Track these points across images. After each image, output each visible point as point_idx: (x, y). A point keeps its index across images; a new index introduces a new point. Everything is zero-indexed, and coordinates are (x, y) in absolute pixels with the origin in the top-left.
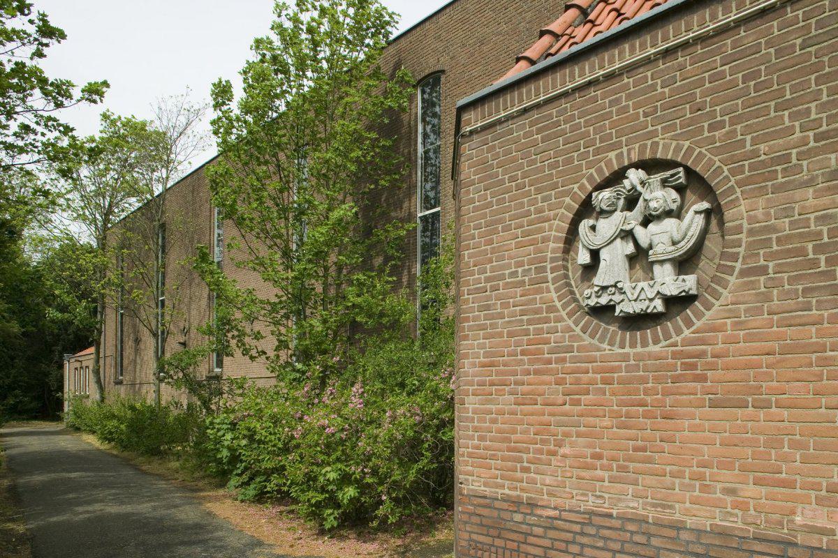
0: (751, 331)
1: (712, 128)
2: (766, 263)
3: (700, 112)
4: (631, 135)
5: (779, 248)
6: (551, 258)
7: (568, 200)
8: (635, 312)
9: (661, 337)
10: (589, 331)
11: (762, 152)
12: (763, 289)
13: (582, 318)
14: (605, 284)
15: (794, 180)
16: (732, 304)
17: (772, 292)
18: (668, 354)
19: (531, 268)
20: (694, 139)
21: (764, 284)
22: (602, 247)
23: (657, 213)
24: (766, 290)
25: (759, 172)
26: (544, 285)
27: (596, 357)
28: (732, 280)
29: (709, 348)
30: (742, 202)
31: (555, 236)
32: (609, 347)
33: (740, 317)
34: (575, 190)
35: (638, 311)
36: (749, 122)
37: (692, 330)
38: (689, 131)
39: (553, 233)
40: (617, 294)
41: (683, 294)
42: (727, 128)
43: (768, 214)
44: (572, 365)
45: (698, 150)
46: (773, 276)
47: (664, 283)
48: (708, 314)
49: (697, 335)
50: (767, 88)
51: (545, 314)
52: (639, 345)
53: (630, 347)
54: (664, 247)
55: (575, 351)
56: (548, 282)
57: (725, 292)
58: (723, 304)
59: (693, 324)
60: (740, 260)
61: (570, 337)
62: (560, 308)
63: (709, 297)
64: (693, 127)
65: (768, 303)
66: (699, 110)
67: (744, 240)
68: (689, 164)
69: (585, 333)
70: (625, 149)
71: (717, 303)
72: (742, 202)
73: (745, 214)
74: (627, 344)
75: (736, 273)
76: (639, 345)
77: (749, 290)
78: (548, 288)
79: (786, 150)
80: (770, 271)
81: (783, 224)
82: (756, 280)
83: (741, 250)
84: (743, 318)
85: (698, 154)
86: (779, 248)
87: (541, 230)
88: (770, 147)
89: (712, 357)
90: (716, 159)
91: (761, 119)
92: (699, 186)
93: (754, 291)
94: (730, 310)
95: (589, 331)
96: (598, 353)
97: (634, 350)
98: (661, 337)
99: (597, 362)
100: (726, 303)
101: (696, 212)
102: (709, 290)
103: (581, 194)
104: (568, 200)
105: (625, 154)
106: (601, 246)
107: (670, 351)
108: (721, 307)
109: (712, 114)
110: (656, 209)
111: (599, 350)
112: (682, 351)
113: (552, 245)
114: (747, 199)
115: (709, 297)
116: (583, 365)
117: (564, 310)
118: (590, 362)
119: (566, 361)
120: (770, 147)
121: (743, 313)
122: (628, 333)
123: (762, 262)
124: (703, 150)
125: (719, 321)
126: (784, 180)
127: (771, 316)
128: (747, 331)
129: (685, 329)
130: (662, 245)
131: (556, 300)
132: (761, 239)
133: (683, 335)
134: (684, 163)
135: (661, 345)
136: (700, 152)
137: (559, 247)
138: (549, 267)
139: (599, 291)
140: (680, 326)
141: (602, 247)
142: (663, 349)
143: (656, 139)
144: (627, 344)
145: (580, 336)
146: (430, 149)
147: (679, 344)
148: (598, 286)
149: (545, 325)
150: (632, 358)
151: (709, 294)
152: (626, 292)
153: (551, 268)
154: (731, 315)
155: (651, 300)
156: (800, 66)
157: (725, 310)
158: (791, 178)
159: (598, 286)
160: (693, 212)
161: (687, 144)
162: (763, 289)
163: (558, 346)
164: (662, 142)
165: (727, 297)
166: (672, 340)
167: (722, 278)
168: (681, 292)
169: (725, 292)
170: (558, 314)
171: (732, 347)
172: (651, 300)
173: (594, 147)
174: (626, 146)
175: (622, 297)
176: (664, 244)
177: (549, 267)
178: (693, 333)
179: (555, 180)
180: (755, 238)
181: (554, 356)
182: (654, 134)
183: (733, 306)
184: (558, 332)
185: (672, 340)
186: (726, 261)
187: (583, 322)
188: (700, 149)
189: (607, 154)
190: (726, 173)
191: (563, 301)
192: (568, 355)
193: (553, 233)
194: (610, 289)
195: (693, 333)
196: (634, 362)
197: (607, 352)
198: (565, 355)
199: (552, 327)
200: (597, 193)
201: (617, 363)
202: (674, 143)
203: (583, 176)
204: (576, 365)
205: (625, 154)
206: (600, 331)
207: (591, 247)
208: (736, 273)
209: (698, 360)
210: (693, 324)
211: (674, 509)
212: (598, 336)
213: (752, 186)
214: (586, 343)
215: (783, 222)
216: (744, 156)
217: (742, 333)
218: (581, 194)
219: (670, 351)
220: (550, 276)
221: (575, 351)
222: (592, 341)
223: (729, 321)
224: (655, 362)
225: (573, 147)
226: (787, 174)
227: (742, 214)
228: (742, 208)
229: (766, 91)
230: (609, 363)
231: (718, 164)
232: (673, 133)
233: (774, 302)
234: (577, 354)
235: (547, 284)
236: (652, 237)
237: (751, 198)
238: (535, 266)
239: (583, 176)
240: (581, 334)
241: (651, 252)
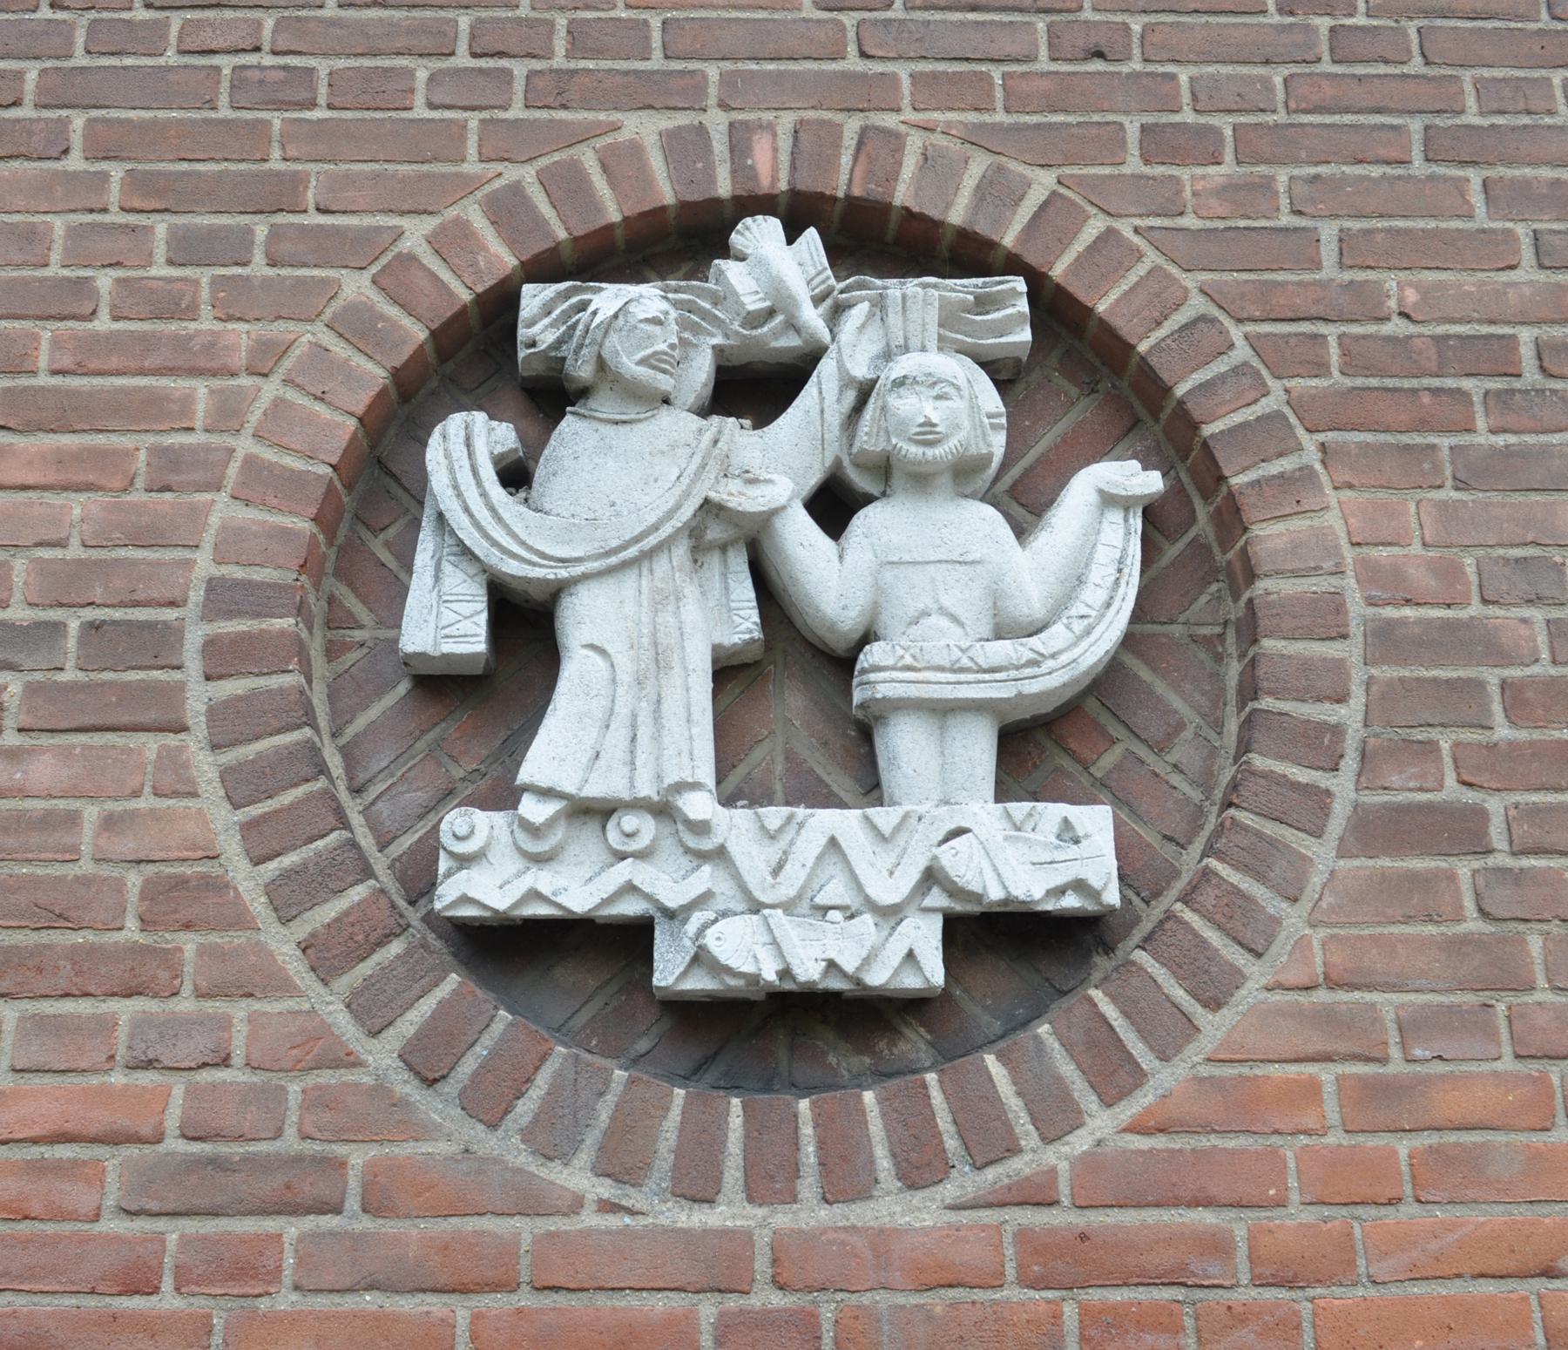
0: (1451, 1138)
1: (1157, 144)
2: (1470, 796)
3: (1098, 66)
4: (753, 66)
5: (1522, 735)
6: (213, 585)
7: (356, 286)
8: (785, 973)
9: (951, 1143)
10: (468, 1066)
11: (1392, 304)
12: (1473, 925)
13: (416, 979)
14: (596, 789)
15: (1545, 450)
16: (1332, 984)
17: (1521, 941)
18: (998, 1247)
19: (58, 628)
20: (1076, 170)
21: (1478, 896)
22: (586, 577)
23: (931, 452)
24: (1488, 928)
25: (1390, 383)
26: (151, 745)
27: (508, 1249)
28: (1321, 854)
29: (1239, 1226)
30: (1332, 496)
31: (250, 462)
32: (605, 1189)
33: (1383, 1060)
34: (406, 245)
35: (809, 971)
36: (1323, 170)
37: (1129, 1110)
38: (1051, 126)
39: (245, 445)
40: (669, 852)
41: (1071, 902)
42: (1227, 168)
43: (1452, 572)
44: (322, 1302)
45: (1095, 226)
46: (1509, 862)
47: (959, 832)
48: (1214, 1027)
49: (1160, 1142)
50: (1386, 62)
51: (132, 931)
52: (808, 1186)
53: (753, 1196)
54: (954, 635)
55: (353, 1203)
56: (184, 729)
57: (1293, 918)
58: (1291, 978)
59: (1139, 1077)
60: (1350, 764)
61: (316, 1100)
62: (258, 905)
63: (1213, 936)
64: (1071, 119)
65: (1511, 998)
66: (1100, 55)
67: (1358, 675)
68: (1058, 271)
69: (431, 1083)
70: (717, 122)
71: (1257, 974)
72: (1332, 496)
73: (1349, 554)
74: (733, 1174)
75: (1336, 825)
76: (808, 1186)
77: (1408, 919)
78: (173, 761)
79: (1492, 322)
80: (1497, 834)
81: (1524, 631)
82: (1436, 875)
83: (1350, 715)
84: (1396, 1066)
85: (1093, 248)
86: (1522, 735)
87: (174, 413)
88: (1425, 291)
89: (1259, 1282)
90: (1190, 281)
91: (1376, 171)
92: (1074, 391)
93: (1431, 929)
94: (1328, 1018)
95: (468, 1066)
96: (525, 1229)
97: (782, 1218)
98: (951, 1143)
99: (510, 1286)
100: (1304, 980)
101: (1109, 500)
102: (1208, 897)
103: (445, 275)
104: (356, 286)
105: (720, 146)
106: (578, 570)
107: (1009, 1230)
108: (1277, 997)
109: (1158, 92)
110: (928, 434)
111: (532, 1201)
112: (1083, 1237)
113: (222, 510)
114: (1350, 486)
115: (1213, 936)
116: (407, 1305)
117: (285, 921)
118: (463, 1290)
119: (275, 1274)
120: (1425, 291)
121: (1394, 1037)
122: (736, 1102)
123: (1452, 790)
124: (1125, 228)
125: (1275, 1070)
126: (1500, 440)
127: (1534, 1067)
128: (1432, 1139)
129: (1088, 1100)
130: (944, 622)
131: (232, 848)
132: (1435, 680)
133: (1079, 1142)
134: (1032, 258)
135: (949, 1190)
136: (1110, 232)
137: (285, 534)
138: (195, 636)
139: (551, 823)
140: (1059, 1079)
141: (586, 577)
142: (965, 1217)
143: (889, 121)
144: (733, 1174)
145: (402, 1104)
146: (425, 919)
147: (1064, 1190)
148: (547, 793)
149: (124, 1009)
150: (762, 1265)
151: (1208, 917)
152: (734, 849)
153: (211, 646)
154: (1342, 1047)
155: (891, 914)
156: (1498, 24)
157: (1298, 1014)
158: (1530, 439)
159: (547, 793)
160: (1093, 498)
161: (1043, 183)
162: (1473, 925)
163: (215, 1163)
164: (915, 143)
165: (1302, 944)
166: (1019, 1166)
167: (1272, 843)
168: (1060, 891)
169: (1293, 918)
170: (239, 938)
171: (1363, 1223)
172: (891, 914)
173: (537, 65)
174: (723, 106)
175: (705, 878)
176: (955, 619)
177: (195, 636)
178: (1136, 1128)
179: (276, 164)
180: (1406, 673)
181: (174, 1232)
182: (877, 93)
183: (1342, 996)
184: (225, 1062)
185: (1019, 1166)
186: (1280, 757)
187: (427, 1006)
188: (1111, 222)
189: (616, 116)
190: (1242, 352)
191: (289, 860)
192: (292, 1229)
193: (245, 445)
194: (630, 821)
195: (1136, 1128)
196: (777, 1300)
197: (590, 1219)
198: (270, 1225)
199: (171, 1028)
200: (551, 290)
201: (659, 1304)
202: (978, 166)
203: (469, 185)
204: (349, 1302)
205: (720, 146)
206: (543, 1080)
207: (511, 568)
208: (1336, 825)
209: (1179, 1293)
210: (1139, 1077)
211: (94, 294)
212: (525, 1109)
213: (1369, 437)
214: (442, 1148)
215: (1524, 621)
216: (1317, 301)
217: (1404, 1147)
218: (445, 275)
219: (1009, 1230)
220: (199, 697)
221: (353, 1203)
222: (488, 1142)
223: (1326, 1075)
224: (915, 1299)
225: (411, 32)
226: (1510, 420)
227: (1335, 551)
228: (1333, 519)
229: (1382, 69)
230: (602, 1301)
231: (1197, 305)
232: (972, 117)
233: (1538, 996)
234: (366, 1224)
235: (171, 740)
236: (888, 575)
237: (1365, 487)
238: (90, 614)
239: (469, 185)
240: (405, 1086)
241: (874, 654)
